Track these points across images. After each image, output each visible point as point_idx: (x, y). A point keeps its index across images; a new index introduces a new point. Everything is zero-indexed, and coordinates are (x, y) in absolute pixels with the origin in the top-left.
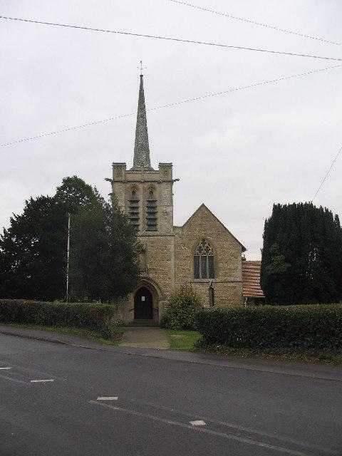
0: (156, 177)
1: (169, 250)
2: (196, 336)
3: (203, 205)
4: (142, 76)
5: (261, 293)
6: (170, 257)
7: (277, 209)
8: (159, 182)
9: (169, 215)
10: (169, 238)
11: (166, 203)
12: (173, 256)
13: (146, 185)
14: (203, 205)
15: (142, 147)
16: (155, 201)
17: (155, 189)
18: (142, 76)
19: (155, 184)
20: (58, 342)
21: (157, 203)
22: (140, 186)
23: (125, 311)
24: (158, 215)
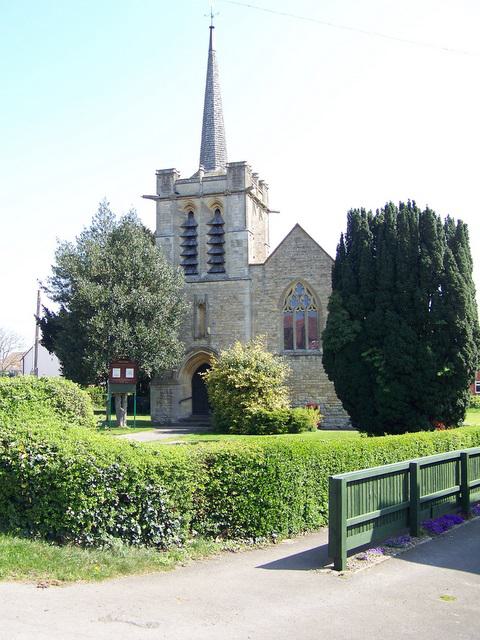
0: (221, 185)
1: (241, 303)
2: (187, 165)
3: (297, 226)
4: (212, 28)
5: (425, 495)
6: (243, 313)
7: (353, 218)
8: (225, 194)
9: (242, 245)
10: (242, 283)
11: (237, 224)
12: (247, 311)
13: (208, 201)
14: (297, 226)
15: (208, 152)
16: (221, 225)
17: (194, 207)
18: (212, 28)
19: (222, 199)
20: (135, 624)
21: (225, 227)
22: (197, 202)
23: (207, 375)
24: (227, 247)
